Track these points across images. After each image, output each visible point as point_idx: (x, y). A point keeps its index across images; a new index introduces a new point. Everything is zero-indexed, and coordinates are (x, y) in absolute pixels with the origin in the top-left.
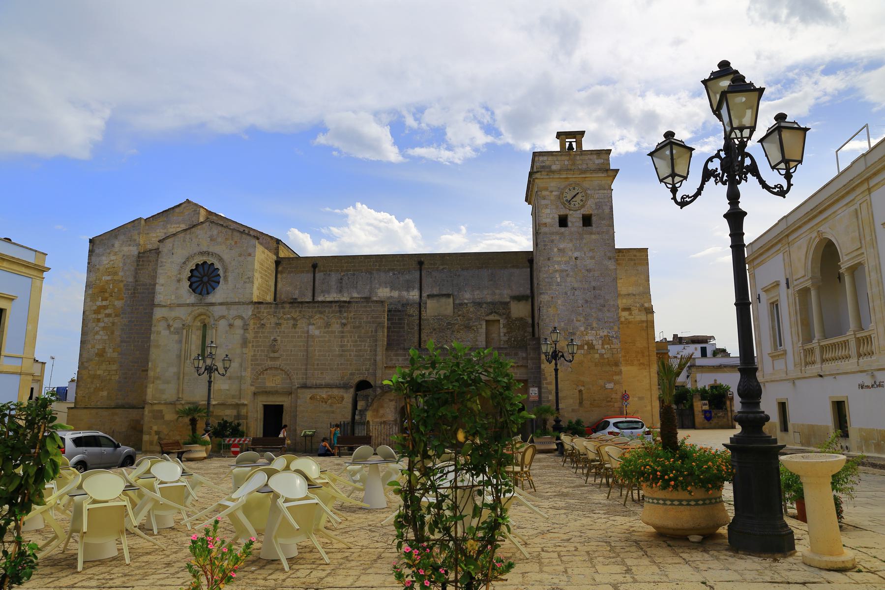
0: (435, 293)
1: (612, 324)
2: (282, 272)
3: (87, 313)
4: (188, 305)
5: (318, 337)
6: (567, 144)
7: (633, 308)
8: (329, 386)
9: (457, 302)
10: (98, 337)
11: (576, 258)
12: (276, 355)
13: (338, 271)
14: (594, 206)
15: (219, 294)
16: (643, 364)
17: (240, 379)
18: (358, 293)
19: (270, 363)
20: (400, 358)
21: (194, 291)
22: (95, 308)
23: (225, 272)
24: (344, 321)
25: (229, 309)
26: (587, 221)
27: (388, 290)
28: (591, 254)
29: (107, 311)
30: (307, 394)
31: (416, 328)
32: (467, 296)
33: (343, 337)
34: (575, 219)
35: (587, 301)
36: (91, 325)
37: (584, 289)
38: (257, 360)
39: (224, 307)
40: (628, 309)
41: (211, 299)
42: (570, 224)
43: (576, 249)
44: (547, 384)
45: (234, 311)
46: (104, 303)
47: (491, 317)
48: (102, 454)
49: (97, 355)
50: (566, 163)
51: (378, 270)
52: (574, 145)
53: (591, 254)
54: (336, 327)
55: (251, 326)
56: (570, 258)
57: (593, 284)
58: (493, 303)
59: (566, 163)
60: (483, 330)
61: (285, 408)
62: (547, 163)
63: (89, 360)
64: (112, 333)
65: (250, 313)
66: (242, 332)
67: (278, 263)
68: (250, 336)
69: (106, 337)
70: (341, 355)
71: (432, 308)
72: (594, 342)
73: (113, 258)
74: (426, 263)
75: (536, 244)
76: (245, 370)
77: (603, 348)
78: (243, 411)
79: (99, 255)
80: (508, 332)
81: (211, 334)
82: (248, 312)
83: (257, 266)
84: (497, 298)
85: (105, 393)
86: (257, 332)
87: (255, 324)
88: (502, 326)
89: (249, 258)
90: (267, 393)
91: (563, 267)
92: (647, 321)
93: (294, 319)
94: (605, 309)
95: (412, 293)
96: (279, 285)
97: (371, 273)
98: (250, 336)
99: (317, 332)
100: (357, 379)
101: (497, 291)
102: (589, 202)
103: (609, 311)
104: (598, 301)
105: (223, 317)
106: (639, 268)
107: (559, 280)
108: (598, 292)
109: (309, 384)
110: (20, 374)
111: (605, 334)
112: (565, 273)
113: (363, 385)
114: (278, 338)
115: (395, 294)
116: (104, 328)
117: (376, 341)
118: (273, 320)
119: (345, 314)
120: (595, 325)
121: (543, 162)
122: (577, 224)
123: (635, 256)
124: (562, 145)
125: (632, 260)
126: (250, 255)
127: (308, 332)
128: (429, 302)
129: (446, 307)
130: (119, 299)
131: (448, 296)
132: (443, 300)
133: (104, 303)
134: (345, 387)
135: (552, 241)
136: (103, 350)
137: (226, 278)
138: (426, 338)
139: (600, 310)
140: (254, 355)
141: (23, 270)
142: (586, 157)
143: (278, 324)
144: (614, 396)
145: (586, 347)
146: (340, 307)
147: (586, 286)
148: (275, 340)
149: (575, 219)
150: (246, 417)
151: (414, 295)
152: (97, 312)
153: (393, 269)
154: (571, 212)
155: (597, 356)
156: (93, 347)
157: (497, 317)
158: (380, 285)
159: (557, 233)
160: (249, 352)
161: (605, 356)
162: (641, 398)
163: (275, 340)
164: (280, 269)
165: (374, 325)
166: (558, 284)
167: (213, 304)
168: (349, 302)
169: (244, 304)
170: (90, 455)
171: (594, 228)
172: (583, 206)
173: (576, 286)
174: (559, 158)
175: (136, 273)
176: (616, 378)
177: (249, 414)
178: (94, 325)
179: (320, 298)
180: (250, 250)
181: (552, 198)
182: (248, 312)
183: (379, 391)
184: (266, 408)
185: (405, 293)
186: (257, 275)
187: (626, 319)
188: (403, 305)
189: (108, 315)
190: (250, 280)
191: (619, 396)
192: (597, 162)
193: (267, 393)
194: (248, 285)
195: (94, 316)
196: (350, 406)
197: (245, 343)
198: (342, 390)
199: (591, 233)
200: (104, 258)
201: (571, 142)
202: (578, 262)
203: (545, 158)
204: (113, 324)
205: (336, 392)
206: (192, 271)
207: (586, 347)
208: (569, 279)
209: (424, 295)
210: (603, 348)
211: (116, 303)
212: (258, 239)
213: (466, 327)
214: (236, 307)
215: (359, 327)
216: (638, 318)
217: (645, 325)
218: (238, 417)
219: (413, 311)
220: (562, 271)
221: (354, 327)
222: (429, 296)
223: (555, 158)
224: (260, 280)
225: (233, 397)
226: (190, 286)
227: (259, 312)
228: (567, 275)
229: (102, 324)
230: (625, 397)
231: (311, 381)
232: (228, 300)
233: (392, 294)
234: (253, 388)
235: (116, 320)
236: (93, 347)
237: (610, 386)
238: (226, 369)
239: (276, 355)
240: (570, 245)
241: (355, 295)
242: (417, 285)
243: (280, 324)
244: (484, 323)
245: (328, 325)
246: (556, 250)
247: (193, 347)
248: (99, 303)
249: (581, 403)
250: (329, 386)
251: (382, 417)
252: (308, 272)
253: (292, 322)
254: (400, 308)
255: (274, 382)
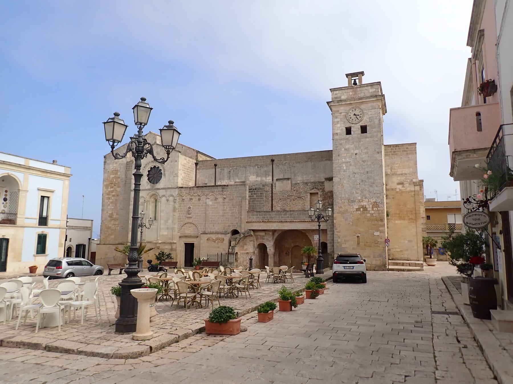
0: (281, 178)
1: (379, 195)
2: (199, 169)
3: (104, 195)
4: (147, 190)
5: (211, 205)
6: (353, 81)
7: (405, 183)
8: (217, 233)
9: (293, 182)
10: (109, 207)
11: (356, 154)
12: (190, 216)
13: (228, 167)
14: (368, 120)
15: (162, 184)
16: (412, 219)
17: (173, 229)
18: (239, 179)
19: (187, 220)
20: (255, 217)
21: (150, 182)
22: (108, 192)
23: (164, 171)
24: (224, 196)
25: (166, 191)
26: (364, 129)
27: (255, 177)
28: (366, 151)
29: (113, 194)
30: (206, 237)
31: (270, 199)
32: (299, 179)
33: (224, 205)
34: (356, 129)
35: (362, 181)
36: (106, 201)
37: (361, 173)
38: (181, 219)
39: (164, 190)
40: (401, 183)
41: (158, 186)
42: (352, 132)
43: (356, 148)
44: (337, 232)
45: (169, 192)
46: (112, 189)
47: (313, 191)
48: (83, 269)
49: (109, 216)
50: (351, 93)
51: (250, 166)
52: (357, 81)
53: (366, 151)
54: (220, 200)
55: (178, 200)
56: (352, 154)
57: (367, 170)
58: (314, 183)
59: (351, 93)
60: (308, 199)
61: (195, 245)
62: (339, 95)
63: (106, 219)
64: (116, 205)
65: (177, 193)
66: (173, 203)
67: (196, 164)
68: (177, 206)
69: (113, 207)
70: (223, 216)
71: (279, 186)
72: (367, 206)
73: (115, 165)
74: (276, 160)
75: (334, 144)
76: (175, 224)
77: (373, 210)
78: (174, 246)
79: (108, 164)
80: (323, 200)
81: (159, 204)
82: (176, 192)
83: (180, 167)
84: (317, 180)
85: (113, 237)
86: (181, 204)
87: (179, 199)
88: (319, 196)
89: (176, 163)
90: (186, 237)
91: (348, 160)
92: (415, 191)
93: (199, 196)
94: (374, 185)
95: (268, 178)
96: (198, 177)
97: (245, 167)
98: (177, 206)
99: (210, 203)
100: (232, 229)
101: (317, 175)
102: (365, 118)
103: (377, 186)
104: (370, 180)
105: (164, 196)
106: (410, 156)
107: (345, 168)
108: (370, 174)
109: (206, 232)
110: (59, 228)
111: (374, 201)
112: (349, 164)
113: (235, 232)
114: (191, 207)
115: (259, 179)
116: (112, 203)
117: (241, 207)
118: (189, 197)
119: (225, 193)
120: (367, 195)
121: (336, 94)
122: (357, 132)
123: (407, 148)
124: (349, 82)
125: (405, 151)
126: (176, 161)
127: (206, 203)
128: (277, 183)
129: (286, 186)
130: (118, 187)
131: (288, 179)
132: (285, 182)
133: (112, 189)
134: (225, 233)
135: (341, 144)
136: (112, 214)
137: (165, 175)
138: (276, 204)
139: (371, 186)
140: (179, 216)
141: (58, 177)
142: (364, 89)
143: (191, 199)
144: (379, 240)
145: (362, 209)
146: (223, 188)
147: (362, 172)
148: (190, 208)
149: (356, 129)
150: (176, 250)
151: (269, 179)
152: (108, 194)
153: (257, 165)
154: (353, 125)
155: (369, 215)
156: (107, 213)
157: (317, 191)
158: (250, 174)
159: (344, 139)
160: (177, 214)
161: (374, 215)
162: (410, 241)
163: (190, 208)
164: (198, 167)
165: (240, 198)
166: (344, 171)
167: (159, 189)
168: (227, 186)
169: (174, 188)
170: (76, 269)
171: (368, 134)
172: (361, 121)
173: (356, 171)
174: (346, 91)
175: (126, 173)
176: (381, 229)
177: (177, 248)
178: (107, 201)
179: (218, 183)
180: (176, 159)
181: (342, 117)
182: (176, 192)
183: (242, 236)
184: (186, 244)
185: (264, 178)
186: (180, 172)
187: (400, 190)
188: (263, 186)
189: (114, 196)
190: (177, 175)
191: (383, 240)
192: (371, 91)
193: (186, 237)
194: (176, 178)
195: (107, 196)
196: (228, 244)
197: (174, 210)
198: (223, 235)
199: (366, 138)
200: (111, 166)
201: (355, 80)
202: (357, 156)
203: (337, 92)
204: (116, 200)
205: (220, 236)
206: (149, 171)
207: (362, 209)
208: (351, 168)
209: (275, 179)
210: (373, 210)
211: (117, 189)
212: (180, 152)
213: (298, 197)
214: (170, 190)
215: (232, 199)
216: (409, 189)
217: (413, 193)
218: (172, 249)
219: (268, 188)
220: (347, 162)
221: (230, 200)
222: (277, 180)
223: (344, 91)
224: (183, 175)
225: (170, 239)
226: (148, 179)
227: (181, 193)
228: (350, 165)
229: (111, 201)
230: (387, 241)
231: (208, 230)
232: (167, 187)
233: (257, 179)
234: (179, 234)
235: (117, 198)
236: (107, 213)
237: (377, 234)
238: (150, 225)
239: (190, 216)
240: (353, 146)
241: (237, 180)
242: (271, 174)
243: (192, 199)
244: (309, 195)
245: (216, 199)
246: (343, 149)
247: (150, 212)
248: (109, 190)
249: (358, 244)
250: (217, 233)
251: (246, 250)
252: (212, 168)
253: (198, 197)
254: (261, 187)
255: (189, 231)
